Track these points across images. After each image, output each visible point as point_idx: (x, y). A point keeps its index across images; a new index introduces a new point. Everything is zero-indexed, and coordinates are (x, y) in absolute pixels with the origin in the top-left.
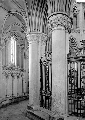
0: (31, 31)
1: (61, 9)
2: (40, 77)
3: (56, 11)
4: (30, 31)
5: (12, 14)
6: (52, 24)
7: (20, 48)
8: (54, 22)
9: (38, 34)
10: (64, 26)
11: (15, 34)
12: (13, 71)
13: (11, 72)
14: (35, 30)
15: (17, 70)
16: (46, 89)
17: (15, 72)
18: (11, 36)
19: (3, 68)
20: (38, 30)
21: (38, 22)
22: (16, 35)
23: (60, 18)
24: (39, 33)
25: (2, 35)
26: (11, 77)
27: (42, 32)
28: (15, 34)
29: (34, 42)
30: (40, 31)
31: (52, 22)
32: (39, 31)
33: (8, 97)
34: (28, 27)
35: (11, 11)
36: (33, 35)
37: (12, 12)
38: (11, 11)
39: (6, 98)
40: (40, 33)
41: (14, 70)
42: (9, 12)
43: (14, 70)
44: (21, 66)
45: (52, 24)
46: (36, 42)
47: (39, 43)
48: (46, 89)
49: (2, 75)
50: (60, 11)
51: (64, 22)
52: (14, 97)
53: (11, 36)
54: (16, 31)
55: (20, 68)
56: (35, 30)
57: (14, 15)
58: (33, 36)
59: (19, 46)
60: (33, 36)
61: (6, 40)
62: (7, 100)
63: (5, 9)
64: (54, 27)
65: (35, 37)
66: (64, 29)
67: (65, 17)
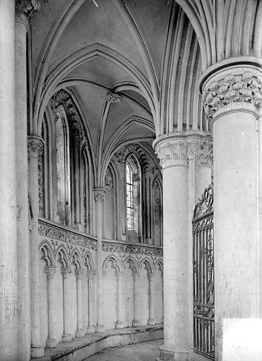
0: (165, 133)
1: (237, 49)
2: (194, 264)
3: (219, 58)
4: (162, 133)
5: (119, 94)
6: (211, 101)
7: (153, 186)
8: (222, 98)
9: (185, 137)
10: (247, 99)
11: (137, 149)
12: (134, 256)
13: (146, 258)
14: (175, 126)
15: (146, 250)
16: (208, 300)
17: (139, 256)
18: (127, 157)
19: (105, 247)
20: (184, 125)
21: (185, 99)
22: (140, 152)
23: (231, 77)
24: (187, 133)
25: (100, 158)
26: (146, 272)
27: (199, 127)
28: (137, 149)
29: (175, 162)
30: (191, 126)
31: (210, 96)
32: (188, 127)
33: (122, 326)
34: (158, 121)
35: (116, 87)
36: (172, 142)
37: (119, 89)
38: (116, 87)
39: (116, 328)
40: (191, 133)
41: (136, 250)
42: (112, 91)
43: (136, 250)
44: (91, 223)
45: (211, 101)
46: (181, 162)
47: (190, 165)
48: (208, 300)
49: (103, 267)
50: (231, 55)
51: (248, 85)
52: (138, 329)
53: (127, 157)
54: (138, 140)
55: (153, 244)
56: (175, 126)
57: (126, 96)
58: (172, 145)
59: (152, 181)
60: (169, 146)
61: (113, 168)
62: (117, 335)
63: (100, 86)
64: (216, 108)
65: (178, 147)
66: (251, 107)
67: (249, 70)
